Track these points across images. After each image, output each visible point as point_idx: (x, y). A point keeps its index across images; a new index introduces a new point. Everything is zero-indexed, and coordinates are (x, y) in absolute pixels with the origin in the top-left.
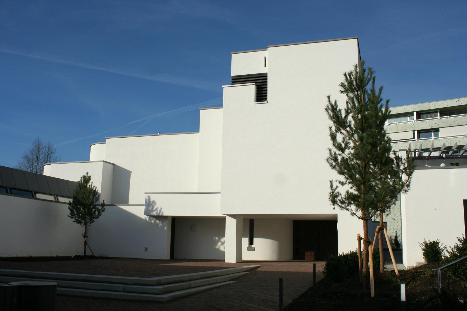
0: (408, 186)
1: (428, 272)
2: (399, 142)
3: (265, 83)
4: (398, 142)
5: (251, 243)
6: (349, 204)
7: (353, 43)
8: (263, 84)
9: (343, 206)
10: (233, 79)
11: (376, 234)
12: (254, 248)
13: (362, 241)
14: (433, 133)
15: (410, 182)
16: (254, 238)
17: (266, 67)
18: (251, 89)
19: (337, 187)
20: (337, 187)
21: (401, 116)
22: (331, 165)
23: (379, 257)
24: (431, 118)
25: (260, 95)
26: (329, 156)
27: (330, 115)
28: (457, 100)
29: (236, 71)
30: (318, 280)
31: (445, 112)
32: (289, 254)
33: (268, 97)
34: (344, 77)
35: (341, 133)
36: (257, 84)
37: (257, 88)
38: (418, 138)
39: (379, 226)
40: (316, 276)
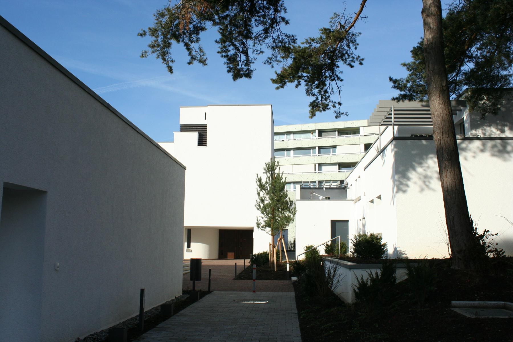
0: (293, 220)
3: (205, 132)
5: (189, 246)
6: (265, 228)
7: (268, 109)
8: (203, 132)
9: (263, 229)
10: (181, 127)
11: (278, 242)
12: (191, 250)
13: (271, 246)
15: (294, 218)
16: (191, 243)
17: (205, 119)
18: (195, 135)
19: (260, 220)
20: (260, 220)
22: (257, 208)
23: (279, 255)
24: (330, 137)
25: (201, 140)
26: (256, 204)
27: (258, 184)
28: (352, 122)
29: (184, 121)
30: (246, 267)
31: (343, 132)
32: (216, 254)
33: (207, 142)
34: (265, 165)
35: (263, 192)
36: (199, 132)
37: (199, 135)
38: (318, 153)
39: (279, 237)
40: (237, 269)
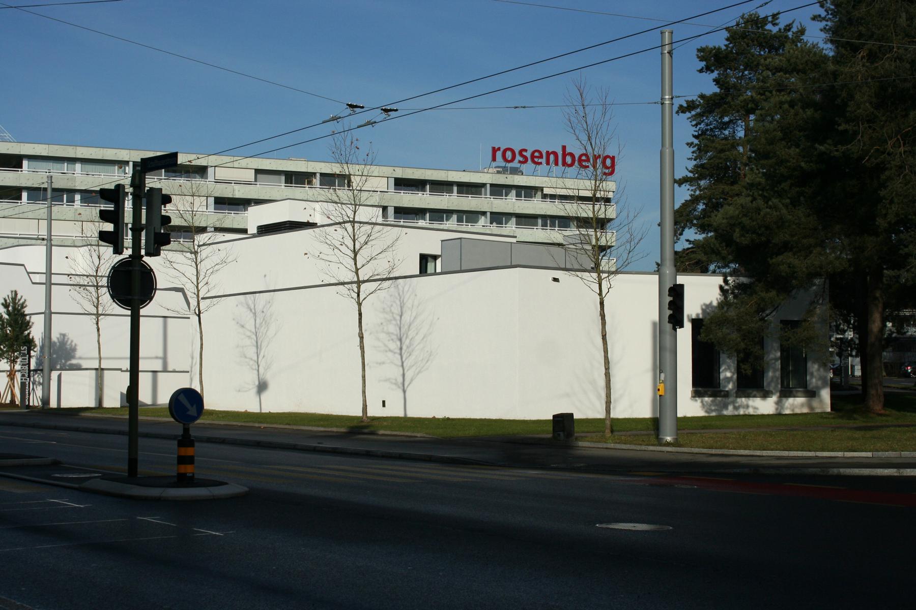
1: (831, 67)
2: (234, 183)
4: (232, 183)
14: (65, 196)
21: (807, 459)
